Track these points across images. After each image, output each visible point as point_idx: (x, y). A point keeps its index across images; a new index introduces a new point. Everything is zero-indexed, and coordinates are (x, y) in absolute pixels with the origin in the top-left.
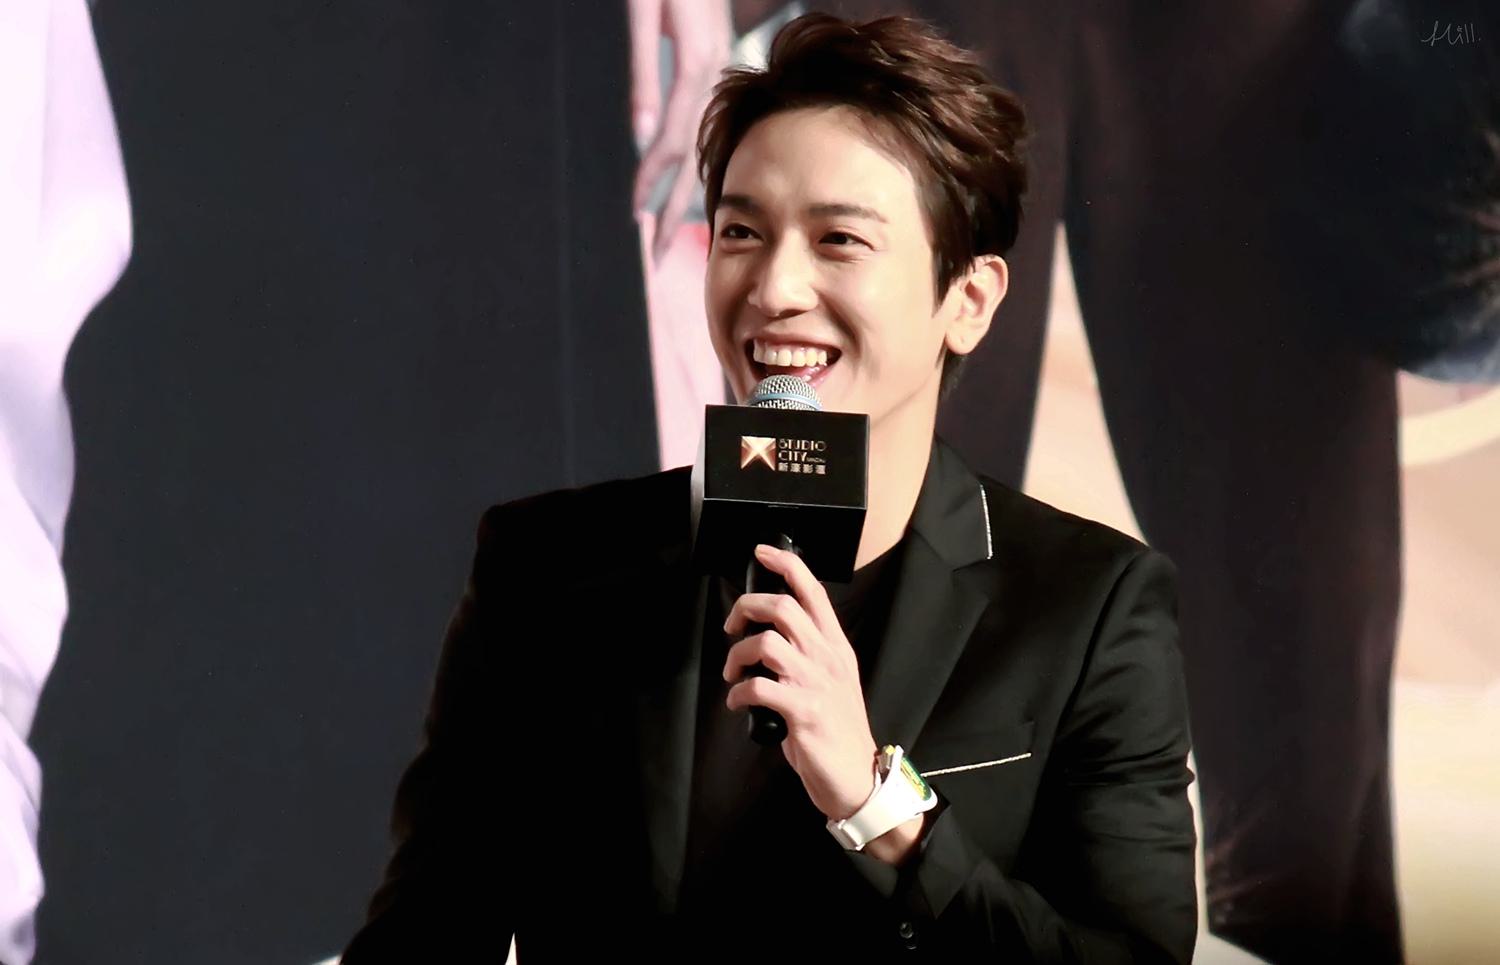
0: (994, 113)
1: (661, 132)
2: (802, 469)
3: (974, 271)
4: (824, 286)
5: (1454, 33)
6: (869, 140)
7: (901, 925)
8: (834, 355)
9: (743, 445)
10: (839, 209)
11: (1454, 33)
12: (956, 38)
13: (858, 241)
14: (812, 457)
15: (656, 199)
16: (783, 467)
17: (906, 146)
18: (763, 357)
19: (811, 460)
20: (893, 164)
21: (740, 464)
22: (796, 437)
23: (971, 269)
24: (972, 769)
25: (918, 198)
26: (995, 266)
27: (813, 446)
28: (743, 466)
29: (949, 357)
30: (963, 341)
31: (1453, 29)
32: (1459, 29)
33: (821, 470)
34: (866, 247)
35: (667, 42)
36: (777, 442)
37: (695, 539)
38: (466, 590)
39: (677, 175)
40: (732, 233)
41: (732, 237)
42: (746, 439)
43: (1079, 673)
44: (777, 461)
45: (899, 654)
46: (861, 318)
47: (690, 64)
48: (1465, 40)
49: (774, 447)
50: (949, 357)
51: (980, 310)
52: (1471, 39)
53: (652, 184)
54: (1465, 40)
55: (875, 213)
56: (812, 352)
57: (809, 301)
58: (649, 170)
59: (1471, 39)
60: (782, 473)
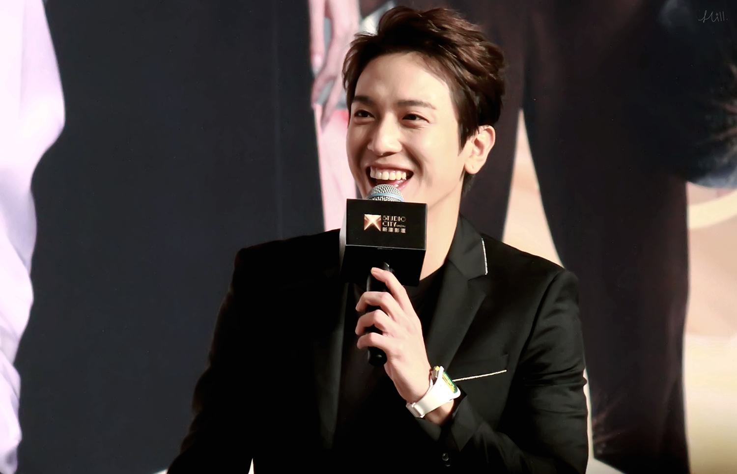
0: (489, 56)
1: (325, 65)
2: (394, 230)
3: (479, 133)
4: (405, 140)
5: (714, 16)
6: (427, 69)
7: (443, 454)
8: (410, 174)
9: (365, 219)
10: (412, 103)
11: (714, 16)
12: (470, 19)
13: (422, 118)
14: (399, 224)
15: (322, 98)
16: (384, 229)
17: (445, 72)
18: (375, 175)
19: (399, 226)
20: (439, 80)
21: (363, 228)
22: (391, 215)
23: (477, 132)
24: (478, 378)
25: (451, 97)
26: (489, 131)
27: (400, 219)
28: (365, 229)
29: (466, 175)
30: (473, 167)
31: (714, 14)
32: (717, 14)
33: (403, 231)
34: (426, 121)
35: (328, 21)
36: (382, 217)
37: (341, 265)
38: (229, 290)
39: (333, 86)
40: (360, 114)
41: (360, 116)
42: (367, 215)
43: (530, 330)
44: (382, 226)
45: (441, 321)
46: (423, 156)
47: (339, 32)
48: (720, 20)
49: (380, 220)
50: (466, 175)
51: (482, 152)
52: (723, 19)
53: (320, 90)
54: (720, 20)
55: (430, 104)
56: (399, 173)
57: (397, 148)
58: (319, 84)
59: (723, 19)
60: (384, 232)
